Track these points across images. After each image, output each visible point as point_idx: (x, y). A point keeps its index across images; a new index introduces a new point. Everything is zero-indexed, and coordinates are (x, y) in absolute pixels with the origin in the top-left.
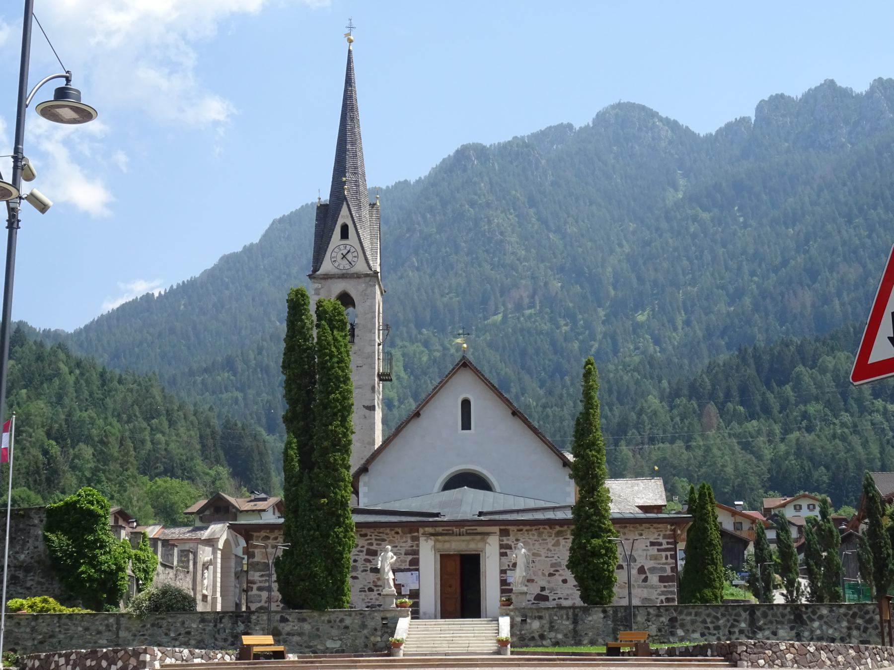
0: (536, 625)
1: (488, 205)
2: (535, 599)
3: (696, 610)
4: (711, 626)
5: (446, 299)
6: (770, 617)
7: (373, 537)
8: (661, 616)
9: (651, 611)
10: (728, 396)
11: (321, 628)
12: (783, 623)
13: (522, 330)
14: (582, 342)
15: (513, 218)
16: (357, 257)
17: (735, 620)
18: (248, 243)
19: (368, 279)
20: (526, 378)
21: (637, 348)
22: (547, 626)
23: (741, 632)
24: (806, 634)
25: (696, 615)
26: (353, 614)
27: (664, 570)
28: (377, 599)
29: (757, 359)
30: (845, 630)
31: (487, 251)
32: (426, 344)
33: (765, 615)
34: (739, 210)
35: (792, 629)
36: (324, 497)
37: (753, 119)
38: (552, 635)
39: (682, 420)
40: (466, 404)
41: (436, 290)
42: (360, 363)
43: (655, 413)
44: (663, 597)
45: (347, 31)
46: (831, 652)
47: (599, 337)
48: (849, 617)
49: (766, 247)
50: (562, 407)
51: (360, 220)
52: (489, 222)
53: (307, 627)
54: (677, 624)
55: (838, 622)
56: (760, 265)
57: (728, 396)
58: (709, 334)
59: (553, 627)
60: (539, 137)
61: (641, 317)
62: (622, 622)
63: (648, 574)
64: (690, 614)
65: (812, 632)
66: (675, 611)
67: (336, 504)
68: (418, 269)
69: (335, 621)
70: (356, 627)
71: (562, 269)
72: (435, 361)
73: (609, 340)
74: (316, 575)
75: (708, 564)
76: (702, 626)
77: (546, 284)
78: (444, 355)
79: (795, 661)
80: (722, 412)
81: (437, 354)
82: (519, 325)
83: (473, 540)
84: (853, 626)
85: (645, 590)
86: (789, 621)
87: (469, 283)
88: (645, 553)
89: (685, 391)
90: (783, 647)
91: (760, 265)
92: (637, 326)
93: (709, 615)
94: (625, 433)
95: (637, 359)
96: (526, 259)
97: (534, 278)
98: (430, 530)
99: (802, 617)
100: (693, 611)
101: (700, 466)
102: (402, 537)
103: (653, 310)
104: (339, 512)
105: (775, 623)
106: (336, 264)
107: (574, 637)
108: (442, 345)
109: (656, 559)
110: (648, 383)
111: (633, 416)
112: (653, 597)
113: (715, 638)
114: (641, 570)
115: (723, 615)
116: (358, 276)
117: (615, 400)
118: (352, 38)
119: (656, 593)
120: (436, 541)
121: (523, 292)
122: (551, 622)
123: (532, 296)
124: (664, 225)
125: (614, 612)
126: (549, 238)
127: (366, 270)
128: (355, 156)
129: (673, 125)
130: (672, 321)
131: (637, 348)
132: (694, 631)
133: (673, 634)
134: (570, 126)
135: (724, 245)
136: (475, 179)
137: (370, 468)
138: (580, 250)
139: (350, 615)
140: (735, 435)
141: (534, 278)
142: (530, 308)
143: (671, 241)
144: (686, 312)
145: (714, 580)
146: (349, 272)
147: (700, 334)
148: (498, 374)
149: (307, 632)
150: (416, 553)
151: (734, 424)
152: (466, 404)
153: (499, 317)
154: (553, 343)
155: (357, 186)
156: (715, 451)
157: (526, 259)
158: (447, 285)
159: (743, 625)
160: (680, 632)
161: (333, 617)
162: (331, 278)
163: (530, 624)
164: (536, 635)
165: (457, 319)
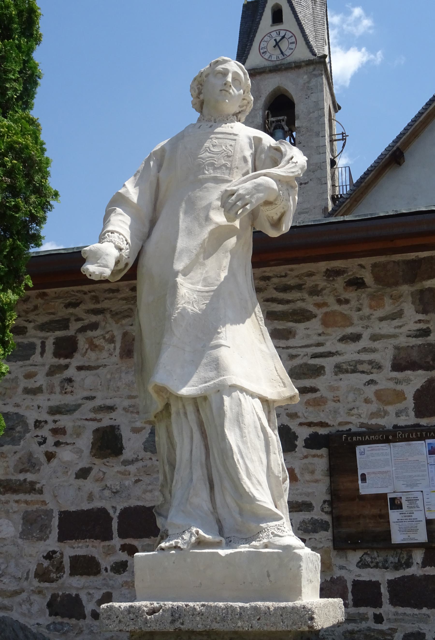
19: (311, 68)
102: (376, 300)
106: (267, 56)
116: (297, 66)
146: (285, 62)
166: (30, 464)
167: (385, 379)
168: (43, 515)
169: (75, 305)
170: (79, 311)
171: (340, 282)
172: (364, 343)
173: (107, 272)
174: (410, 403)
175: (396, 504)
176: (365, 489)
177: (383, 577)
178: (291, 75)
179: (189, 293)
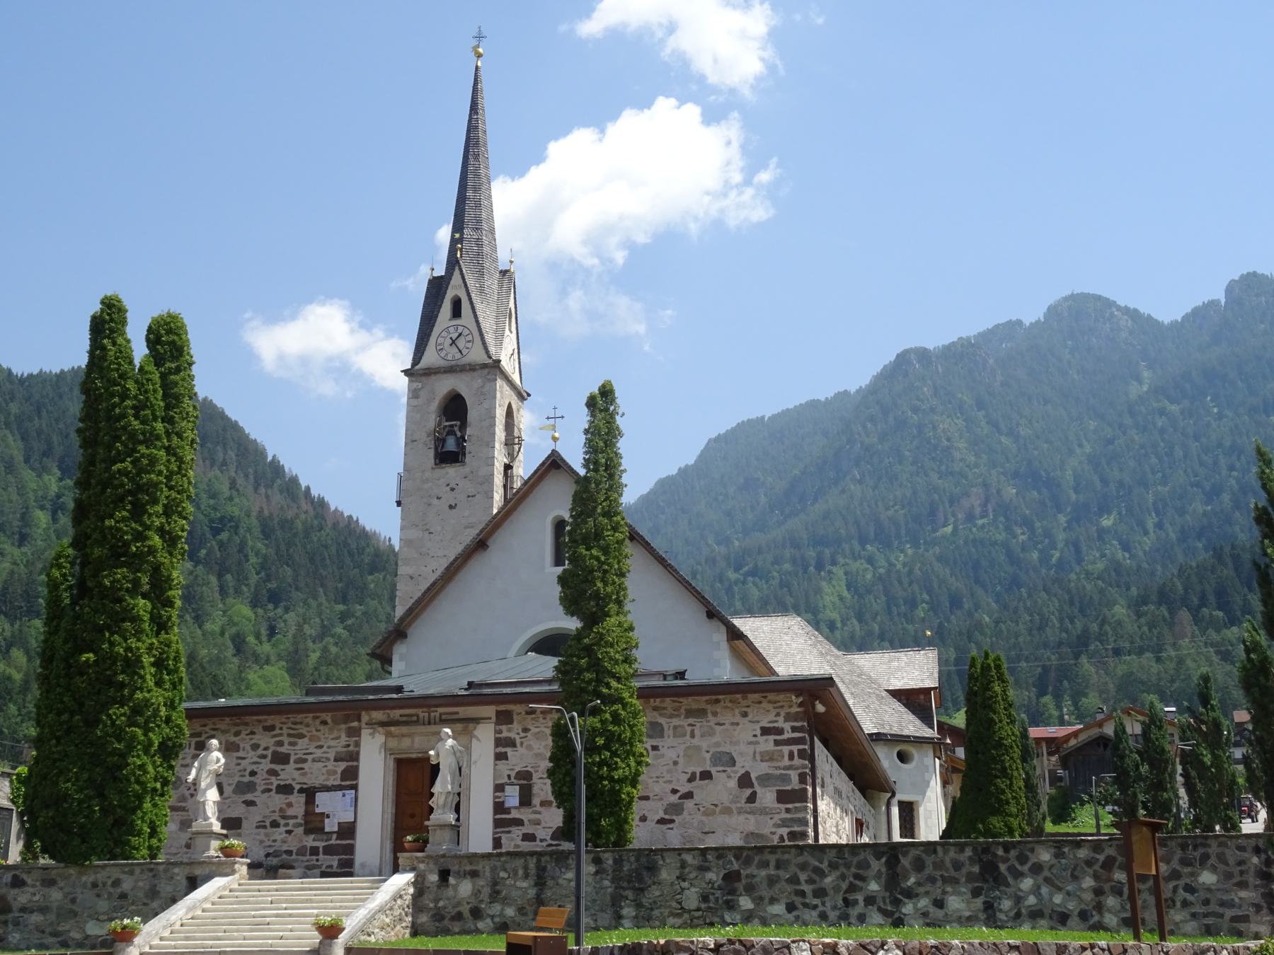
0: (465, 888)
1: (933, 410)
2: (552, 839)
4: (807, 888)
5: (890, 513)
6: (929, 870)
7: (285, 731)
8: (708, 869)
9: (688, 858)
10: (1203, 602)
11: (80, 897)
13: (974, 541)
14: (1041, 552)
15: (960, 422)
16: (472, 341)
17: (857, 877)
18: (683, 466)
19: (486, 371)
20: (980, 592)
21: (1103, 555)
22: (486, 891)
23: (870, 900)
24: (1006, 904)
25: (778, 867)
26: (137, 871)
27: (785, 779)
28: (284, 842)
29: (1236, 558)
30: (1088, 896)
31: (933, 459)
32: (871, 561)
33: (919, 865)
34: (1212, 401)
35: (976, 893)
36: (92, 650)
37: (1223, 301)
38: (496, 908)
39: (1150, 630)
41: (880, 504)
42: (471, 491)
43: (1119, 623)
44: (784, 831)
45: (474, 42)
47: (1060, 545)
48: (1097, 867)
49: (1245, 438)
50: (1017, 622)
51: (481, 290)
52: (934, 428)
53: (56, 895)
54: (740, 886)
55: (1075, 878)
56: (1239, 459)
57: (1203, 602)
58: (1184, 535)
59: (498, 892)
60: (987, 336)
61: (1107, 522)
62: (629, 882)
63: (757, 788)
64: (765, 865)
65: (1018, 900)
66: (737, 858)
67: (114, 663)
68: (860, 482)
69: (104, 884)
70: (141, 894)
71: (1016, 475)
72: (880, 578)
73: (1072, 548)
74: (66, 796)
75: (997, 777)
76: (789, 888)
77: (999, 491)
78: (889, 572)
80: (1197, 620)
81: (882, 571)
82: (971, 537)
84: (1107, 887)
85: (751, 817)
86: (970, 878)
87: (915, 493)
88: (752, 747)
89: (1154, 598)
91: (1239, 459)
92: (1102, 532)
93: (803, 867)
94: (1087, 645)
95: (1100, 566)
96: (976, 465)
97: (986, 485)
98: (378, 715)
99: (998, 867)
100: (772, 859)
101: (1173, 681)
103: (1119, 514)
104: (121, 678)
105: (939, 883)
108: (888, 561)
109: (771, 759)
110: (1113, 592)
111: (1094, 627)
112: (766, 831)
113: (815, 913)
114: (745, 781)
115: (833, 866)
116: (472, 368)
117: (1076, 611)
118: (481, 50)
119: (771, 823)
120: (388, 735)
121: (974, 501)
122: (495, 883)
123: (985, 505)
124: (1128, 421)
125: (615, 861)
126: (1000, 442)
127: (483, 359)
128: (478, 205)
129: (1134, 314)
130: (1141, 524)
131: (1103, 555)
132: (773, 900)
133: (731, 906)
134: (1019, 322)
135: (1196, 438)
136: (917, 384)
137: (411, 632)
138: (1036, 453)
139: (131, 873)
140: (1212, 645)
141: (986, 485)
142: (982, 517)
143: (1136, 438)
144: (1158, 514)
145: (1008, 803)
146: (460, 363)
147: (1173, 536)
148: (948, 590)
149: (55, 905)
150: (354, 757)
151: (1211, 632)
153: (949, 529)
154: (1010, 554)
155: (480, 246)
156: (1189, 662)
157: (976, 465)
158: (891, 497)
159: (874, 886)
160: (746, 903)
161: (101, 876)
162: (435, 373)
163: (455, 887)
164: (465, 909)
165: (903, 532)
167: (331, 765)
168: (1145, 807)
169: (205, 726)
170: (206, 729)
171: (318, 722)
172: (325, 749)
174: (339, 776)
175: (328, 816)
176: (317, 810)
177: (321, 844)
178: (465, 377)
179: (203, 785)
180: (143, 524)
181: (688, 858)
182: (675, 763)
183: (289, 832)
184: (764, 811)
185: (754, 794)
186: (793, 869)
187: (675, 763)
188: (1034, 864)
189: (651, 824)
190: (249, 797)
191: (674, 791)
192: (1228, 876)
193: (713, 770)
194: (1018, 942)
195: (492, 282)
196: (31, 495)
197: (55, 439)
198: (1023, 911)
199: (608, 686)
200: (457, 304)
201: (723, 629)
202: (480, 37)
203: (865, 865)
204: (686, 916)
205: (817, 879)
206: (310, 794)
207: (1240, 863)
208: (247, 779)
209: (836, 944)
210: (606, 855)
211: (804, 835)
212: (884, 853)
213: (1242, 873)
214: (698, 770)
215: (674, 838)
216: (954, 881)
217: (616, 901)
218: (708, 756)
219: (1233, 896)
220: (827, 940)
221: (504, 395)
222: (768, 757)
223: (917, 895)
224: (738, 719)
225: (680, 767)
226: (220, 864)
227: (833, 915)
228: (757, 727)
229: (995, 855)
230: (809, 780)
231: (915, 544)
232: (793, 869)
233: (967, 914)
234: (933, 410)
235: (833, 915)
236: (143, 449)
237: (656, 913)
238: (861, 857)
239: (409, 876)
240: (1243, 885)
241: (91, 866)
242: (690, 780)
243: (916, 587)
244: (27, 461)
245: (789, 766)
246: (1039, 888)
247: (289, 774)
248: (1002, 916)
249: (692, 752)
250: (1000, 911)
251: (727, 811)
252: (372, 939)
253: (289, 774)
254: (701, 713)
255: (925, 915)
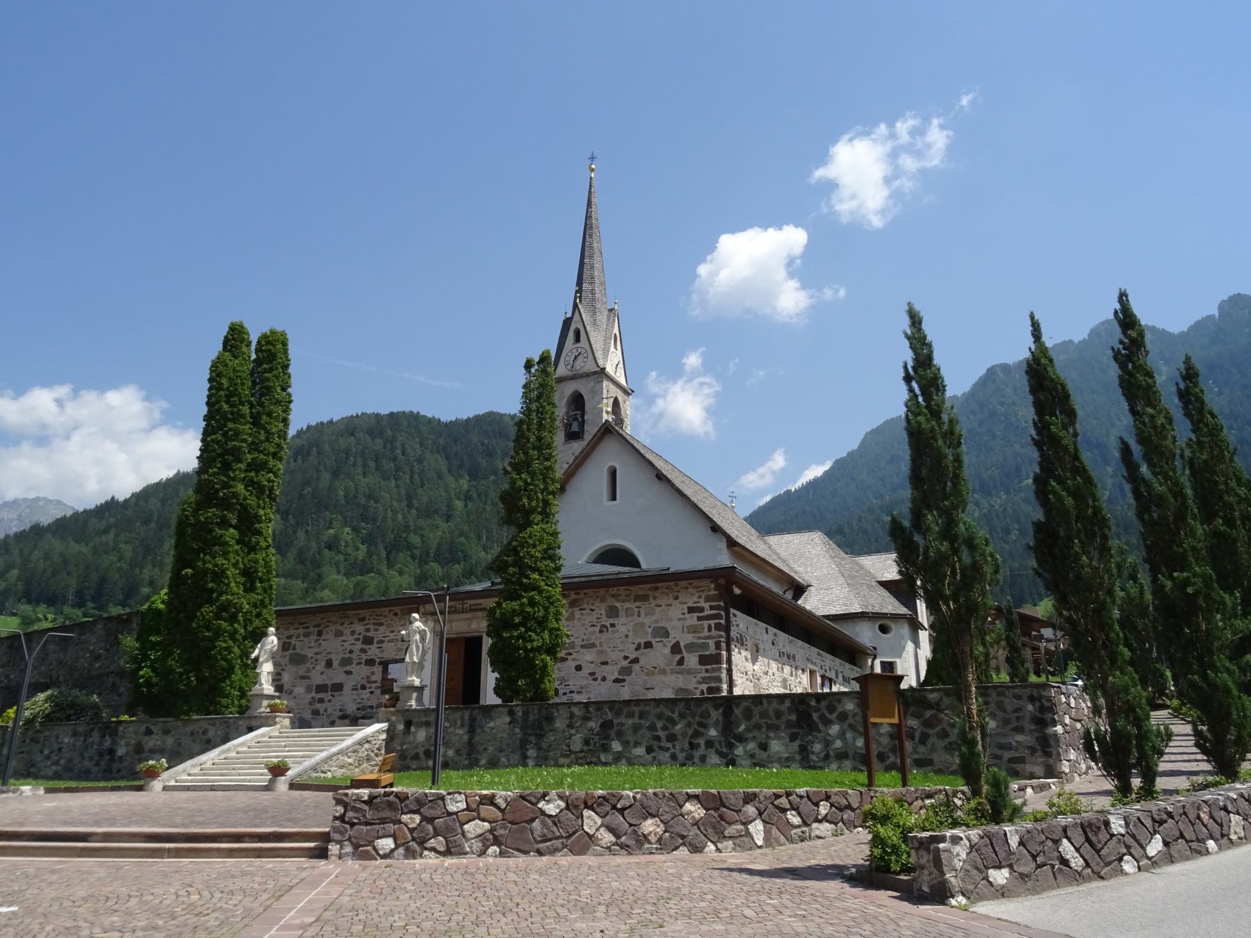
0: (421, 735)
3: (641, 708)
4: (662, 734)
5: (989, 472)
9: (575, 710)
12: (777, 728)
23: (709, 744)
24: (817, 747)
27: (705, 646)
33: (748, 715)
35: (793, 738)
40: (613, 473)
44: (704, 687)
46: (622, 811)
47: (1109, 487)
51: (594, 323)
52: (1016, 415)
54: (612, 733)
63: (685, 654)
65: (827, 743)
66: (611, 709)
67: (206, 575)
74: (171, 671)
76: (648, 734)
79: (491, 838)
83: (474, 618)
86: (789, 725)
90: (456, 805)
93: (659, 717)
99: (811, 716)
100: (636, 710)
104: (210, 585)
105: (764, 729)
107: (469, 754)
109: (695, 632)
112: (691, 687)
113: (667, 755)
114: (676, 649)
115: (682, 716)
116: (587, 375)
125: (524, 712)
132: (636, 744)
133: (606, 748)
134: (1071, 342)
139: (214, 725)
152: (613, 473)
159: (713, 732)
160: (616, 746)
163: (416, 733)
164: (421, 751)
166: (308, 671)
173: (936, 162)
180: (228, 477)
181: (575, 710)
182: (627, 636)
183: (372, 693)
184: (689, 672)
185: (683, 658)
186: (652, 718)
187: (627, 636)
188: (840, 713)
189: (609, 682)
190: (348, 668)
191: (626, 658)
192: (1006, 722)
193: (653, 641)
194: (698, 791)
195: (602, 317)
196: (452, 492)
197: (465, 458)
198: (831, 753)
199: (527, 577)
200: (577, 333)
201: (724, 540)
202: (592, 158)
203: (706, 715)
204: (573, 756)
205: (669, 726)
206: (385, 665)
207: (1017, 710)
208: (347, 656)
209: (493, 796)
210: (519, 708)
211: (719, 690)
212: (721, 705)
213: (1018, 718)
214: (643, 641)
215: (625, 693)
216: (776, 728)
217: (523, 745)
218: (650, 630)
219: (1010, 740)
220: (485, 792)
221: (609, 391)
222: (693, 630)
223: (746, 740)
224: (671, 601)
225: (630, 639)
226: (266, 717)
227: (681, 756)
228: (685, 607)
229: (809, 706)
230: (723, 645)
231: (1008, 493)
232: (652, 718)
233: (786, 755)
234: (1014, 403)
235: (681, 756)
236: (231, 425)
237: (551, 754)
238: (703, 708)
239: (384, 725)
240: (1019, 730)
241: (189, 720)
242: (637, 649)
243: (1009, 520)
244: (450, 471)
245: (708, 635)
246: (844, 733)
247: (373, 651)
248: (814, 758)
249: (639, 627)
250: (813, 753)
251: (663, 672)
252: (329, 775)
253: (373, 651)
254: (645, 598)
255: (752, 756)
